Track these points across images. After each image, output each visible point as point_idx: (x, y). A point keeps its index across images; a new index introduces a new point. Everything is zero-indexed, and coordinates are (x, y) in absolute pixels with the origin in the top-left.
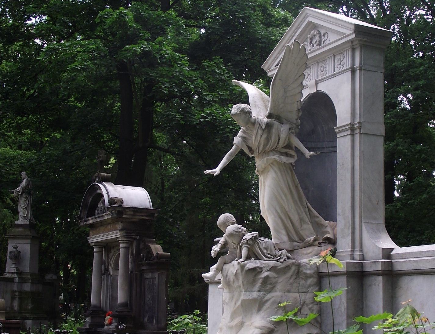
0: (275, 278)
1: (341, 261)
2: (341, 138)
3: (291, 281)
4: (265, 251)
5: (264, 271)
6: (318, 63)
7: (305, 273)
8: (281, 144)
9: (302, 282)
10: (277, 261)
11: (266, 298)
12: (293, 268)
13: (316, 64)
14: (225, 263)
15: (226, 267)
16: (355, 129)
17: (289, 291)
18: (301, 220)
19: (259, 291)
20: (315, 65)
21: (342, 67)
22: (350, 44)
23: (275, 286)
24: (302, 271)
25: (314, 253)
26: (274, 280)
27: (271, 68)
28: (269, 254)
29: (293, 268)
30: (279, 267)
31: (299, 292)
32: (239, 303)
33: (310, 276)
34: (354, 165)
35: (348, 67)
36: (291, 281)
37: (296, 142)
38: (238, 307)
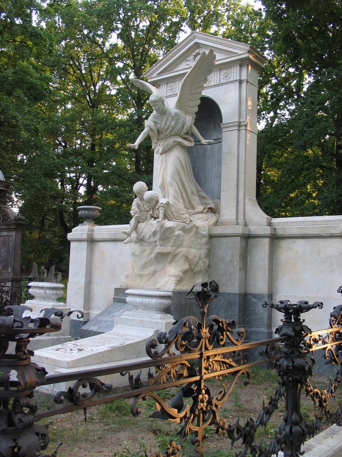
0: (183, 236)
1: (124, 242)
2: (229, 132)
3: (193, 239)
4: (175, 214)
5: (176, 230)
6: (220, 70)
7: (201, 233)
8: (184, 131)
9: (199, 240)
10: (184, 222)
11: (177, 252)
12: (194, 229)
13: (219, 71)
14: (139, 222)
15: (141, 226)
16: (241, 126)
17: (191, 247)
18: (192, 193)
19: (172, 246)
20: (217, 72)
21: (228, 79)
22: (240, 62)
23: (182, 243)
24: (199, 232)
25: (204, 218)
26: (182, 238)
27: (151, 75)
28: (177, 217)
29: (194, 229)
30: (186, 228)
31: (196, 249)
32: (153, 255)
33: (203, 236)
34: (237, 155)
35: (235, 79)
36: (193, 239)
37: (195, 130)
38: (151, 259)
